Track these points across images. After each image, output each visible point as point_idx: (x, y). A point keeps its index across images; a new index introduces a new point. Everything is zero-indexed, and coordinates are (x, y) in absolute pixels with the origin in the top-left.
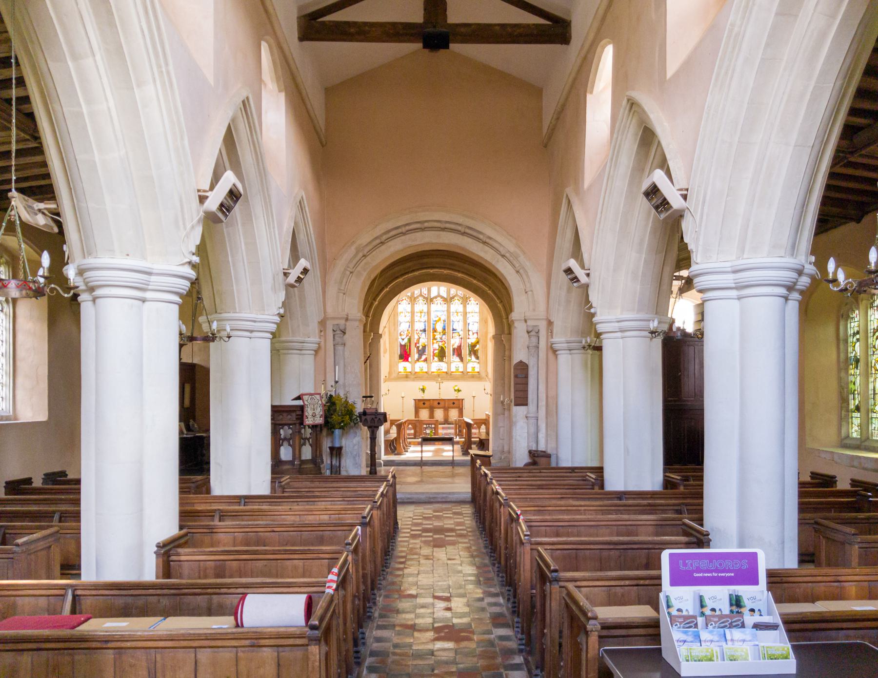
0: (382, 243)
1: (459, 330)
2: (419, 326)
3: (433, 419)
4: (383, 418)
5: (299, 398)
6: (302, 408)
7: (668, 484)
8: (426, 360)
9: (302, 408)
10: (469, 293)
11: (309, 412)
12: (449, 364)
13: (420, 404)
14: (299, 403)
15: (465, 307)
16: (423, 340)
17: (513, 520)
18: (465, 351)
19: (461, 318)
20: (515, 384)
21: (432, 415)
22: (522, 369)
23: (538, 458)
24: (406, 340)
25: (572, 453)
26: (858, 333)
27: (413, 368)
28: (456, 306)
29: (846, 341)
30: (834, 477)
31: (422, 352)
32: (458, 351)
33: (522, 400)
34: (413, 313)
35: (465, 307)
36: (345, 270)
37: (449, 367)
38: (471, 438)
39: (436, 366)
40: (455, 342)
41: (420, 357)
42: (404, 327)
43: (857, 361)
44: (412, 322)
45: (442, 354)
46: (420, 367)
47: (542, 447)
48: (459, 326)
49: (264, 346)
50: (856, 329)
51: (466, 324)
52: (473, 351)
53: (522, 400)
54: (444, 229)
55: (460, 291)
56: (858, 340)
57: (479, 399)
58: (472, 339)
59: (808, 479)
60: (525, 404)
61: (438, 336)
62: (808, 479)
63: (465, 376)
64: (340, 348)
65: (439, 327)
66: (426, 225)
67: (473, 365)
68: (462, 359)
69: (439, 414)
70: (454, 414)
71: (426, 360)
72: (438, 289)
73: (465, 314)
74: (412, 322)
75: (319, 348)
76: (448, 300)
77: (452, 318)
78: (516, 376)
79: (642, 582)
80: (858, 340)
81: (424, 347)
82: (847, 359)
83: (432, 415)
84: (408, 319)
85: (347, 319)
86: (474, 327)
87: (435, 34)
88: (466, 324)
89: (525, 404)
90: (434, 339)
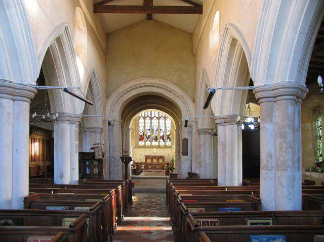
0: (129, 92)
1: (163, 130)
2: (147, 128)
3: (155, 163)
4: (130, 159)
5: (92, 148)
6: (94, 154)
7: (244, 184)
8: (150, 141)
9: (94, 154)
10: (167, 115)
11: (97, 154)
12: (159, 142)
13: (147, 157)
14: (92, 151)
15: (165, 121)
16: (149, 133)
17: (229, 132)
18: (165, 138)
19: (164, 125)
20: (183, 147)
21: (152, 161)
22: (185, 141)
23: (192, 175)
24: (142, 133)
25: (204, 173)
26: (321, 126)
27: (145, 144)
28: (162, 121)
29: (316, 129)
30: (314, 181)
31: (148, 138)
32: (162, 138)
33: (185, 153)
34: (145, 123)
35: (165, 121)
36: (113, 102)
37: (159, 143)
38: (168, 168)
39: (155, 143)
40: (162, 134)
41: (148, 139)
42: (141, 128)
43: (320, 137)
44: (145, 126)
45: (156, 139)
46: (148, 143)
47: (193, 171)
48: (163, 128)
49: (75, 128)
50: (320, 125)
51: (165, 127)
52: (168, 137)
53: (185, 153)
54: (154, 86)
55: (162, 113)
56: (321, 129)
57: (169, 152)
58: (168, 133)
59: (304, 182)
60: (186, 154)
61: (155, 132)
62: (304, 182)
63: (165, 147)
64: (112, 132)
65: (155, 129)
66: (146, 84)
67: (169, 143)
68: (164, 141)
69: (155, 161)
70: (161, 161)
71: (150, 141)
72: (155, 112)
73: (165, 124)
74: (145, 126)
75: (102, 131)
76: (159, 118)
77: (160, 125)
78: (183, 144)
79: (224, 216)
80: (321, 129)
81: (149, 136)
82: (316, 136)
83: (152, 161)
84: (143, 125)
85: (114, 121)
86: (169, 129)
87: (149, 9)
88: (165, 127)
89: (186, 154)
90: (153, 133)
